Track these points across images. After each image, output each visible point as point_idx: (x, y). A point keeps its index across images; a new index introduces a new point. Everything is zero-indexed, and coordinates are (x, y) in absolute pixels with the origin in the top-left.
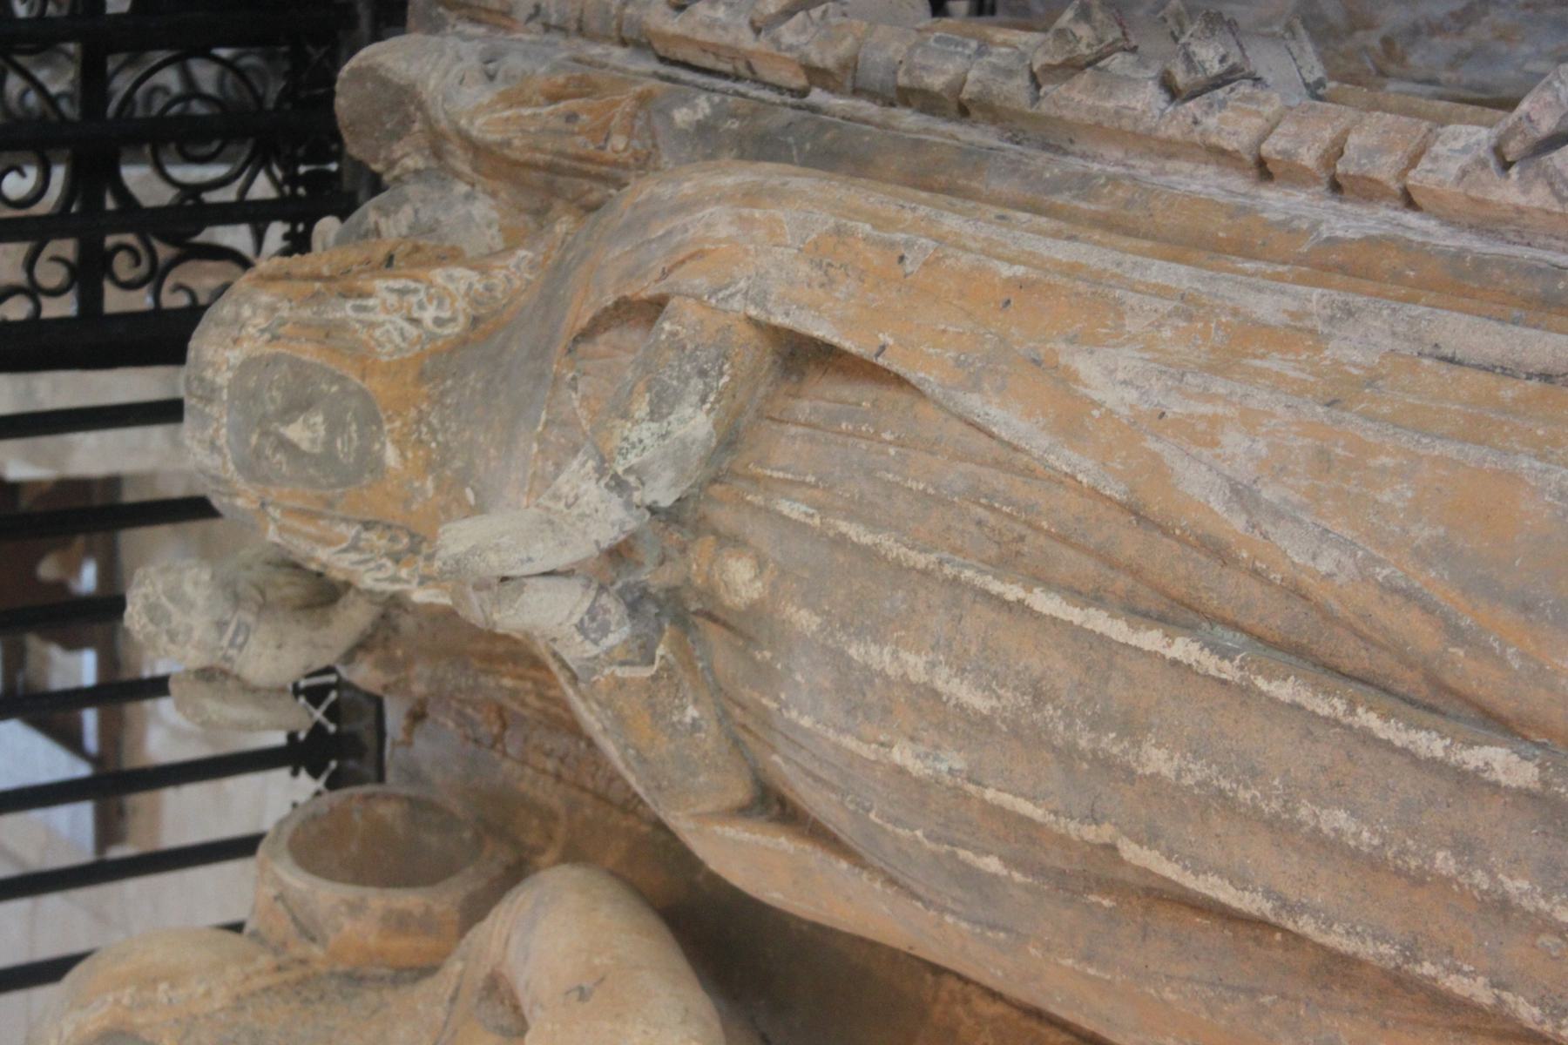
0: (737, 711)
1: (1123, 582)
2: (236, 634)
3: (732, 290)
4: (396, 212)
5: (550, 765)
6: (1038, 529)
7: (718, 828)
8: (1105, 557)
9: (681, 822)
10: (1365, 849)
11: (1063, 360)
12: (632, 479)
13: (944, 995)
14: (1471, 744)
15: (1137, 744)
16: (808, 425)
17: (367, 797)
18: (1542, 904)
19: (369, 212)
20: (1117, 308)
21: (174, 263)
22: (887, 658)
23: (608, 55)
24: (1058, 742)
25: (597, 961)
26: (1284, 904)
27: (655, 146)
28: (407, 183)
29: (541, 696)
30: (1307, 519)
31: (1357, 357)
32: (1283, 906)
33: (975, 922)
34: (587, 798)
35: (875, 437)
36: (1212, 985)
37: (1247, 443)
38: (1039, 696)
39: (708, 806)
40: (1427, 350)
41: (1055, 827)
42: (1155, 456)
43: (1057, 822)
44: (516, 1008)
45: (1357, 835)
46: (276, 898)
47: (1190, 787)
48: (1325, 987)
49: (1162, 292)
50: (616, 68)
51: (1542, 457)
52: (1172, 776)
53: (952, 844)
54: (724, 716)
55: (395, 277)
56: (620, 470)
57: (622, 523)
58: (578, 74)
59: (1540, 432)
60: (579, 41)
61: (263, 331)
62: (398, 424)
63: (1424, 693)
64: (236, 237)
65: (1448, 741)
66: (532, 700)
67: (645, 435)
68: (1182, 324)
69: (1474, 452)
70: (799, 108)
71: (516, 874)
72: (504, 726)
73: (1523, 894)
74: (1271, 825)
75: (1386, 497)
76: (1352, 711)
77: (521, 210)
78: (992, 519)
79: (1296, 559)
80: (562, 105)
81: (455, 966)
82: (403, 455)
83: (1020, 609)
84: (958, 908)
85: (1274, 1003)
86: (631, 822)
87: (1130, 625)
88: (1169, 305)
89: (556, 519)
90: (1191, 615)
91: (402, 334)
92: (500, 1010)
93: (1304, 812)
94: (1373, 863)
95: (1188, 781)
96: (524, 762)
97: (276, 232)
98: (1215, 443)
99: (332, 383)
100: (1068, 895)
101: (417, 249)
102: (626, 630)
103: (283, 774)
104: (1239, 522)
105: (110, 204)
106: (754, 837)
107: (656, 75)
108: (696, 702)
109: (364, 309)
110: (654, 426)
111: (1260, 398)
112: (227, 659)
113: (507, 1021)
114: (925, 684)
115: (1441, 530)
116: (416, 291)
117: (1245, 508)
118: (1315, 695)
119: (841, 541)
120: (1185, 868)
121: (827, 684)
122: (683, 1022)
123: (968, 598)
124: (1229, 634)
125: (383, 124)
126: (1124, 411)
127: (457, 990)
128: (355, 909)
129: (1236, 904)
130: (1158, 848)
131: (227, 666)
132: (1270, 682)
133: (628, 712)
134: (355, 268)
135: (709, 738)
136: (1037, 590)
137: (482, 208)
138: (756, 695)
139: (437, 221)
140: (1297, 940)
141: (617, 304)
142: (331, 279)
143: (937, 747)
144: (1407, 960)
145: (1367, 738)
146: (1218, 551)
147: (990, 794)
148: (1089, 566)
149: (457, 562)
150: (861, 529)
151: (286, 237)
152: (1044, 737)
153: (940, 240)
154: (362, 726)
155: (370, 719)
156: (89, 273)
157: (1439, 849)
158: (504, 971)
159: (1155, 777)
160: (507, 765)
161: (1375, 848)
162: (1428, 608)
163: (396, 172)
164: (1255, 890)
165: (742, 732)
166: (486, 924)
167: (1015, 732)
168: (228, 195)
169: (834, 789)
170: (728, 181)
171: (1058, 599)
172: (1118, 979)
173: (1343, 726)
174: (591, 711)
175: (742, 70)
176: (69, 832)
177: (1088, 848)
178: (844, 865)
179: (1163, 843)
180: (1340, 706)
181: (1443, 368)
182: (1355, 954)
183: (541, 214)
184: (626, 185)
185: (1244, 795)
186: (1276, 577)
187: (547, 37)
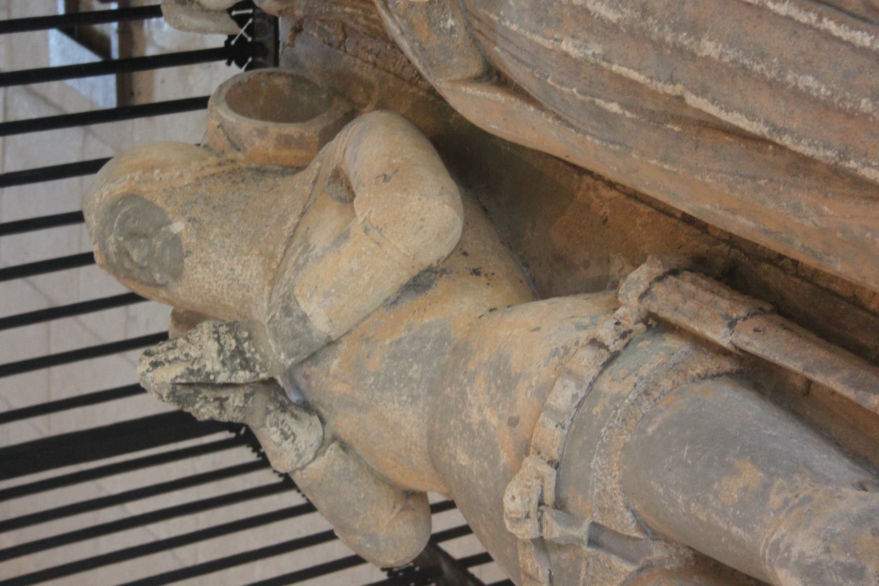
0: (476, 22)
5: (370, 58)
7: (463, 89)
9: (442, 86)
10: (822, 98)
13: (584, 186)
15: (699, 39)
17: (269, 74)
24: (654, 38)
25: (394, 161)
26: (775, 129)
29: (366, 18)
32: (775, 130)
33: (603, 140)
34: (391, 76)
36: (733, 174)
39: (458, 76)
41: (650, 86)
43: (651, 83)
44: (349, 188)
45: (818, 90)
46: (218, 127)
47: (726, 64)
48: (794, 175)
52: (717, 57)
53: (593, 96)
54: (468, 25)
63: (862, 11)
65: (873, 37)
66: (361, 20)
71: (350, 116)
72: (346, 36)
74: (771, 85)
76: (820, 20)
81: (316, 165)
84: (593, 132)
85: (766, 184)
92: (340, 188)
93: (789, 77)
94: (825, 106)
95: (726, 60)
96: (356, 56)
100: (655, 124)
103: (222, 63)
106: (483, 94)
108: (453, 16)
113: (343, 195)
114: (581, 6)
118: (800, 11)
120: (721, 109)
121: (527, 6)
122: (441, 194)
127: (317, 177)
128: (262, 133)
129: (748, 129)
130: (706, 97)
132: (775, 4)
133: (415, 21)
135: (460, 36)
138: (487, 13)
140: (781, 149)
143: (586, 41)
144: (841, 159)
145: (828, 35)
147: (615, 68)
152: (647, 35)
154: (266, 39)
155: (271, 34)
157: (864, 97)
158: (343, 167)
159: (708, 58)
160: (346, 58)
161: (828, 97)
164: (759, 121)
165: (479, 33)
166: (334, 142)
167: (631, 32)
169: (528, 65)
172: (681, 171)
173: (814, 29)
174: (395, 22)
176: (101, 92)
177: (668, 98)
178: (532, 109)
179: (710, 95)
180: (813, 17)
182: (813, 156)
185: (757, 68)
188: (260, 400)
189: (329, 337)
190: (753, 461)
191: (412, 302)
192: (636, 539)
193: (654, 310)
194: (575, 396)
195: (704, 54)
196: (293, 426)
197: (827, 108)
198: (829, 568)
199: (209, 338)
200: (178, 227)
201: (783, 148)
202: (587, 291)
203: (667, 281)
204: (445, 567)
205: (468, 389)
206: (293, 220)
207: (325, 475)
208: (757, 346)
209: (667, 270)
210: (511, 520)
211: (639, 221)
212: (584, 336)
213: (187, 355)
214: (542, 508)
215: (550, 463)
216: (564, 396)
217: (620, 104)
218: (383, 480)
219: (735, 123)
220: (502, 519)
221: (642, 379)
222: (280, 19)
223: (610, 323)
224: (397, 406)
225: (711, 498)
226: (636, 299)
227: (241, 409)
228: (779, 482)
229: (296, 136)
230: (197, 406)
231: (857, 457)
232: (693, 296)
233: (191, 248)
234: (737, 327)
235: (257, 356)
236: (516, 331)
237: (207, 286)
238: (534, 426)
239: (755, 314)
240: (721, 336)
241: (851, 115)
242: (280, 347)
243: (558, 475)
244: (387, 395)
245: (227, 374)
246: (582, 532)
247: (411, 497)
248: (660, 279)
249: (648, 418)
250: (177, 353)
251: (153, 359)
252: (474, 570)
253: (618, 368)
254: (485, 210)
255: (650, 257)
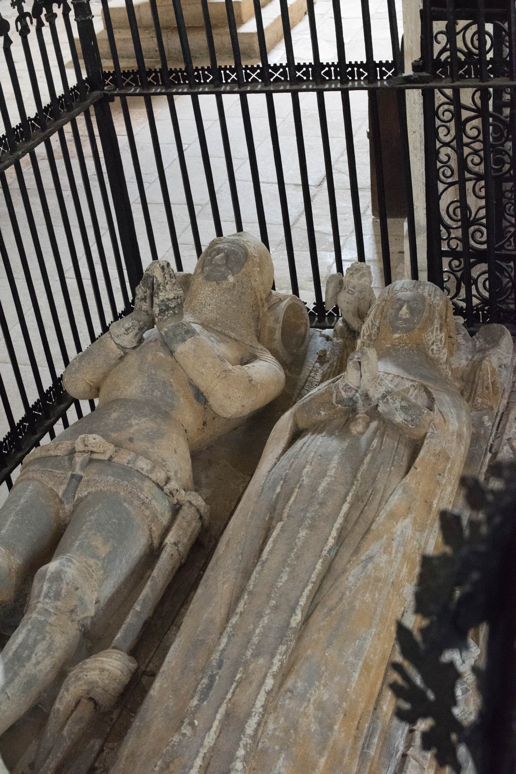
0: (322, 425)
1: (349, 527)
2: (351, 291)
3: (435, 429)
4: (464, 339)
6: (365, 506)
8: (357, 522)
10: (277, 584)
11: (410, 516)
12: (385, 400)
13: (245, 476)
14: (302, 611)
15: (307, 528)
16: (397, 447)
18: (261, 626)
19: (464, 331)
20: (422, 531)
21: (456, 276)
22: (334, 465)
23: (505, 399)
26: (264, 563)
27: (478, 410)
28: (472, 342)
30: (362, 575)
31: (405, 591)
32: (263, 562)
35: (393, 465)
37: (384, 561)
38: (322, 504)
40: (406, 610)
42: (382, 537)
45: (281, 582)
48: (242, 572)
49: (426, 543)
50: (501, 401)
51: (375, 635)
55: (445, 339)
56: (388, 397)
57: (374, 397)
58: (499, 390)
59: (382, 635)
60: (510, 391)
61: (432, 302)
62: (405, 338)
63: (316, 601)
64: (463, 293)
67: (397, 404)
68: (417, 547)
69: (377, 618)
70: (486, 450)
73: (264, 621)
75: (367, 595)
76: (312, 582)
77: (463, 373)
78: (368, 494)
79: (352, 571)
80: (491, 385)
81: (260, 347)
82: (397, 339)
83: (344, 501)
86: (296, 395)
87: (338, 528)
88: (422, 544)
89: (376, 380)
90: (340, 544)
91: (429, 340)
93: (287, 569)
94: (273, 585)
95: (297, 540)
97: (463, 305)
98: (384, 553)
99: (417, 320)
101: (453, 345)
102: (345, 397)
104: (363, 558)
105: (472, 260)
107: (498, 411)
108: (325, 414)
109: (437, 330)
110: (399, 407)
111: (396, 565)
112: (345, 289)
115: (357, 608)
116: (441, 344)
117: (367, 559)
119: (366, 455)
123: (348, 487)
124: (334, 553)
125: (489, 336)
126: (395, 530)
129: (265, 551)
131: (343, 289)
134: (448, 328)
135: (316, 418)
136: (349, 505)
137: (464, 362)
139: (461, 351)
140: (255, 565)
141: (433, 398)
142: (446, 321)
145: (306, 586)
146: (356, 551)
147: (297, 490)
148: (355, 518)
149: (365, 353)
150: (368, 460)
151: (462, 307)
153: (445, 485)
156: (453, 254)
158: (258, 360)
159: (298, 532)
162: (337, 603)
163: (476, 339)
164: (268, 555)
167: (312, 498)
168: (474, 292)
170: (465, 429)
171: (346, 510)
174: (325, 386)
175: (498, 435)
181: (401, 613)
183: (462, 379)
184: (468, 402)
185: (292, 555)
186: (348, 566)
187: (511, 382)
188: (144, 318)
189: (174, 352)
190: (110, 552)
191: (191, 394)
192: (74, 497)
193: (184, 508)
194: (142, 469)
195: (300, 531)
196: (132, 334)
197: (272, 586)
198: (60, 584)
199: (175, 294)
200: (231, 279)
201: (255, 566)
202: (194, 477)
203: (196, 514)
204: (63, 406)
205: (148, 418)
206: (233, 335)
207: (108, 349)
208: (164, 556)
209: (202, 514)
210: (84, 438)
211: (227, 502)
212: (172, 474)
213: (167, 283)
214: (90, 453)
215: (111, 457)
216: (143, 464)
217: (280, 492)
218: (105, 376)
219: (268, 545)
220: (85, 433)
221: (150, 501)
222: (333, 330)
223: (177, 487)
224: (140, 384)
225: (93, 532)
226: (189, 499)
227: (140, 309)
228: (100, 563)
229: (275, 337)
230: (143, 288)
231: (111, 600)
232: (189, 526)
233: (220, 285)
234: (174, 547)
235: (166, 317)
236: (175, 442)
237: (202, 292)
238: (128, 450)
239: (180, 555)
240: (170, 539)
241: (269, 596)
242: (170, 328)
243: (105, 460)
244: (146, 379)
245: (158, 303)
246: (78, 471)
247: (97, 390)
248: (198, 510)
249: (131, 503)
250: (168, 278)
251: (166, 267)
252: (60, 421)
253: (156, 489)
254: (235, 429)
255: (209, 506)
